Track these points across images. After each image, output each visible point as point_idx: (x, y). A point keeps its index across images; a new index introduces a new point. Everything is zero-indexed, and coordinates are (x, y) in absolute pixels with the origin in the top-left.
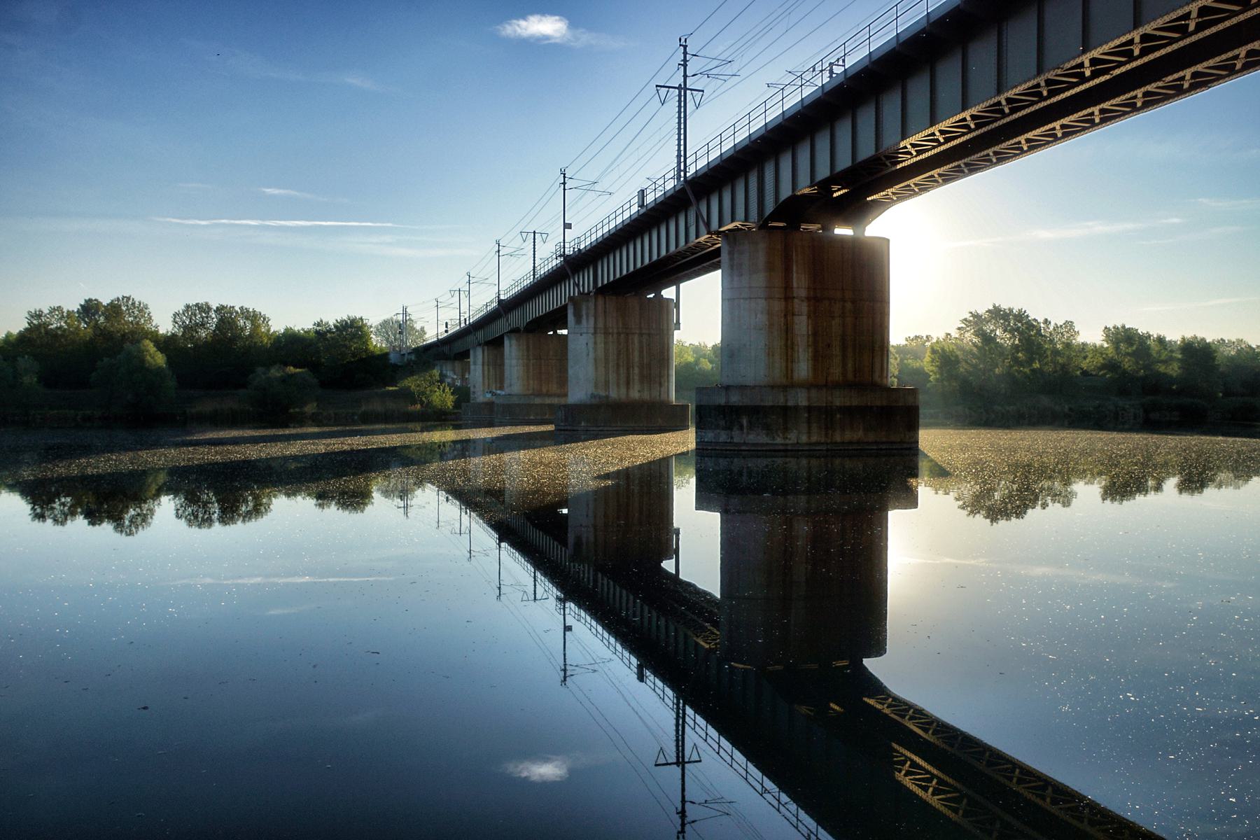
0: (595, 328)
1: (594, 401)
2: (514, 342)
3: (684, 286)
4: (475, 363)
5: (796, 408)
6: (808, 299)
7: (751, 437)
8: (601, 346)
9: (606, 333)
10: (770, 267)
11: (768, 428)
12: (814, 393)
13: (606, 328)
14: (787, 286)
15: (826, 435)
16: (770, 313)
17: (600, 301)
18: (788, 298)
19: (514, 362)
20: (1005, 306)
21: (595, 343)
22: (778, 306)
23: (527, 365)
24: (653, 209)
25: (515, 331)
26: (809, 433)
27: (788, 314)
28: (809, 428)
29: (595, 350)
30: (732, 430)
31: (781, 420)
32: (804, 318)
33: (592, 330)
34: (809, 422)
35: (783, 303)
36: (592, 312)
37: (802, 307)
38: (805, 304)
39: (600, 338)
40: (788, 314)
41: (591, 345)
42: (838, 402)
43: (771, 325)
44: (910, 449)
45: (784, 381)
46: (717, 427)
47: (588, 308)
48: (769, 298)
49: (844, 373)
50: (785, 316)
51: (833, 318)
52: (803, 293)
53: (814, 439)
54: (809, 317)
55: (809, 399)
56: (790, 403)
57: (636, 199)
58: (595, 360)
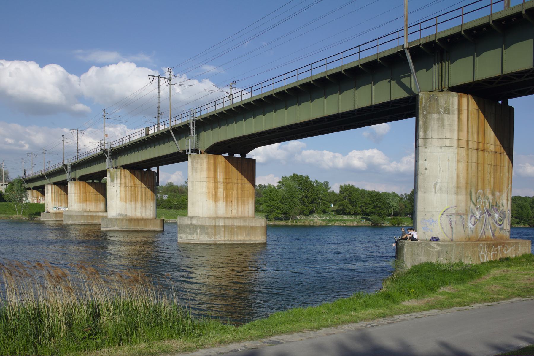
0: (120, 184)
1: (120, 217)
2: (73, 185)
3: (160, 168)
4: (47, 193)
5: (219, 226)
6: (224, 182)
7: (201, 237)
8: (123, 193)
9: (126, 186)
10: (209, 169)
11: (207, 234)
12: (226, 221)
13: (125, 183)
14: (215, 177)
15: (231, 237)
16: (208, 188)
17: (123, 170)
18: (216, 182)
19: (73, 195)
20: (299, 174)
21: (120, 191)
22: (212, 185)
23: (80, 197)
24: (153, 137)
25: (74, 179)
26: (225, 237)
27: (216, 188)
28: (224, 234)
29: (120, 193)
30: (193, 234)
31: (213, 231)
32: (222, 190)
33: (119, 185)
34: (224, 232)
35: (214, 184)
36: (119, 176)
37: (221, 186)
38: (222, 185)
39: (123, 188)
40: (216, 188)
41: (118, 192)
42: (236, 224)
43: (209, 193)
44: (516, 218)
45: (215, 216)
46: (187, 233)
47: (117, 175)
48: (208, 182)
49: (237, 213)
50: (215, 189)
51: (233, 190)
52: (222, 180)
53: (227, 238)
54: (224, 189)
55: (224, 223)
56: (217, 224)
57: (144, 131)
58: (121, 198)
